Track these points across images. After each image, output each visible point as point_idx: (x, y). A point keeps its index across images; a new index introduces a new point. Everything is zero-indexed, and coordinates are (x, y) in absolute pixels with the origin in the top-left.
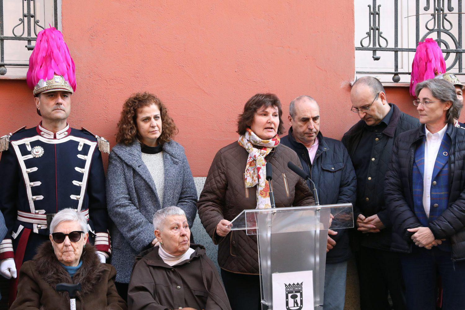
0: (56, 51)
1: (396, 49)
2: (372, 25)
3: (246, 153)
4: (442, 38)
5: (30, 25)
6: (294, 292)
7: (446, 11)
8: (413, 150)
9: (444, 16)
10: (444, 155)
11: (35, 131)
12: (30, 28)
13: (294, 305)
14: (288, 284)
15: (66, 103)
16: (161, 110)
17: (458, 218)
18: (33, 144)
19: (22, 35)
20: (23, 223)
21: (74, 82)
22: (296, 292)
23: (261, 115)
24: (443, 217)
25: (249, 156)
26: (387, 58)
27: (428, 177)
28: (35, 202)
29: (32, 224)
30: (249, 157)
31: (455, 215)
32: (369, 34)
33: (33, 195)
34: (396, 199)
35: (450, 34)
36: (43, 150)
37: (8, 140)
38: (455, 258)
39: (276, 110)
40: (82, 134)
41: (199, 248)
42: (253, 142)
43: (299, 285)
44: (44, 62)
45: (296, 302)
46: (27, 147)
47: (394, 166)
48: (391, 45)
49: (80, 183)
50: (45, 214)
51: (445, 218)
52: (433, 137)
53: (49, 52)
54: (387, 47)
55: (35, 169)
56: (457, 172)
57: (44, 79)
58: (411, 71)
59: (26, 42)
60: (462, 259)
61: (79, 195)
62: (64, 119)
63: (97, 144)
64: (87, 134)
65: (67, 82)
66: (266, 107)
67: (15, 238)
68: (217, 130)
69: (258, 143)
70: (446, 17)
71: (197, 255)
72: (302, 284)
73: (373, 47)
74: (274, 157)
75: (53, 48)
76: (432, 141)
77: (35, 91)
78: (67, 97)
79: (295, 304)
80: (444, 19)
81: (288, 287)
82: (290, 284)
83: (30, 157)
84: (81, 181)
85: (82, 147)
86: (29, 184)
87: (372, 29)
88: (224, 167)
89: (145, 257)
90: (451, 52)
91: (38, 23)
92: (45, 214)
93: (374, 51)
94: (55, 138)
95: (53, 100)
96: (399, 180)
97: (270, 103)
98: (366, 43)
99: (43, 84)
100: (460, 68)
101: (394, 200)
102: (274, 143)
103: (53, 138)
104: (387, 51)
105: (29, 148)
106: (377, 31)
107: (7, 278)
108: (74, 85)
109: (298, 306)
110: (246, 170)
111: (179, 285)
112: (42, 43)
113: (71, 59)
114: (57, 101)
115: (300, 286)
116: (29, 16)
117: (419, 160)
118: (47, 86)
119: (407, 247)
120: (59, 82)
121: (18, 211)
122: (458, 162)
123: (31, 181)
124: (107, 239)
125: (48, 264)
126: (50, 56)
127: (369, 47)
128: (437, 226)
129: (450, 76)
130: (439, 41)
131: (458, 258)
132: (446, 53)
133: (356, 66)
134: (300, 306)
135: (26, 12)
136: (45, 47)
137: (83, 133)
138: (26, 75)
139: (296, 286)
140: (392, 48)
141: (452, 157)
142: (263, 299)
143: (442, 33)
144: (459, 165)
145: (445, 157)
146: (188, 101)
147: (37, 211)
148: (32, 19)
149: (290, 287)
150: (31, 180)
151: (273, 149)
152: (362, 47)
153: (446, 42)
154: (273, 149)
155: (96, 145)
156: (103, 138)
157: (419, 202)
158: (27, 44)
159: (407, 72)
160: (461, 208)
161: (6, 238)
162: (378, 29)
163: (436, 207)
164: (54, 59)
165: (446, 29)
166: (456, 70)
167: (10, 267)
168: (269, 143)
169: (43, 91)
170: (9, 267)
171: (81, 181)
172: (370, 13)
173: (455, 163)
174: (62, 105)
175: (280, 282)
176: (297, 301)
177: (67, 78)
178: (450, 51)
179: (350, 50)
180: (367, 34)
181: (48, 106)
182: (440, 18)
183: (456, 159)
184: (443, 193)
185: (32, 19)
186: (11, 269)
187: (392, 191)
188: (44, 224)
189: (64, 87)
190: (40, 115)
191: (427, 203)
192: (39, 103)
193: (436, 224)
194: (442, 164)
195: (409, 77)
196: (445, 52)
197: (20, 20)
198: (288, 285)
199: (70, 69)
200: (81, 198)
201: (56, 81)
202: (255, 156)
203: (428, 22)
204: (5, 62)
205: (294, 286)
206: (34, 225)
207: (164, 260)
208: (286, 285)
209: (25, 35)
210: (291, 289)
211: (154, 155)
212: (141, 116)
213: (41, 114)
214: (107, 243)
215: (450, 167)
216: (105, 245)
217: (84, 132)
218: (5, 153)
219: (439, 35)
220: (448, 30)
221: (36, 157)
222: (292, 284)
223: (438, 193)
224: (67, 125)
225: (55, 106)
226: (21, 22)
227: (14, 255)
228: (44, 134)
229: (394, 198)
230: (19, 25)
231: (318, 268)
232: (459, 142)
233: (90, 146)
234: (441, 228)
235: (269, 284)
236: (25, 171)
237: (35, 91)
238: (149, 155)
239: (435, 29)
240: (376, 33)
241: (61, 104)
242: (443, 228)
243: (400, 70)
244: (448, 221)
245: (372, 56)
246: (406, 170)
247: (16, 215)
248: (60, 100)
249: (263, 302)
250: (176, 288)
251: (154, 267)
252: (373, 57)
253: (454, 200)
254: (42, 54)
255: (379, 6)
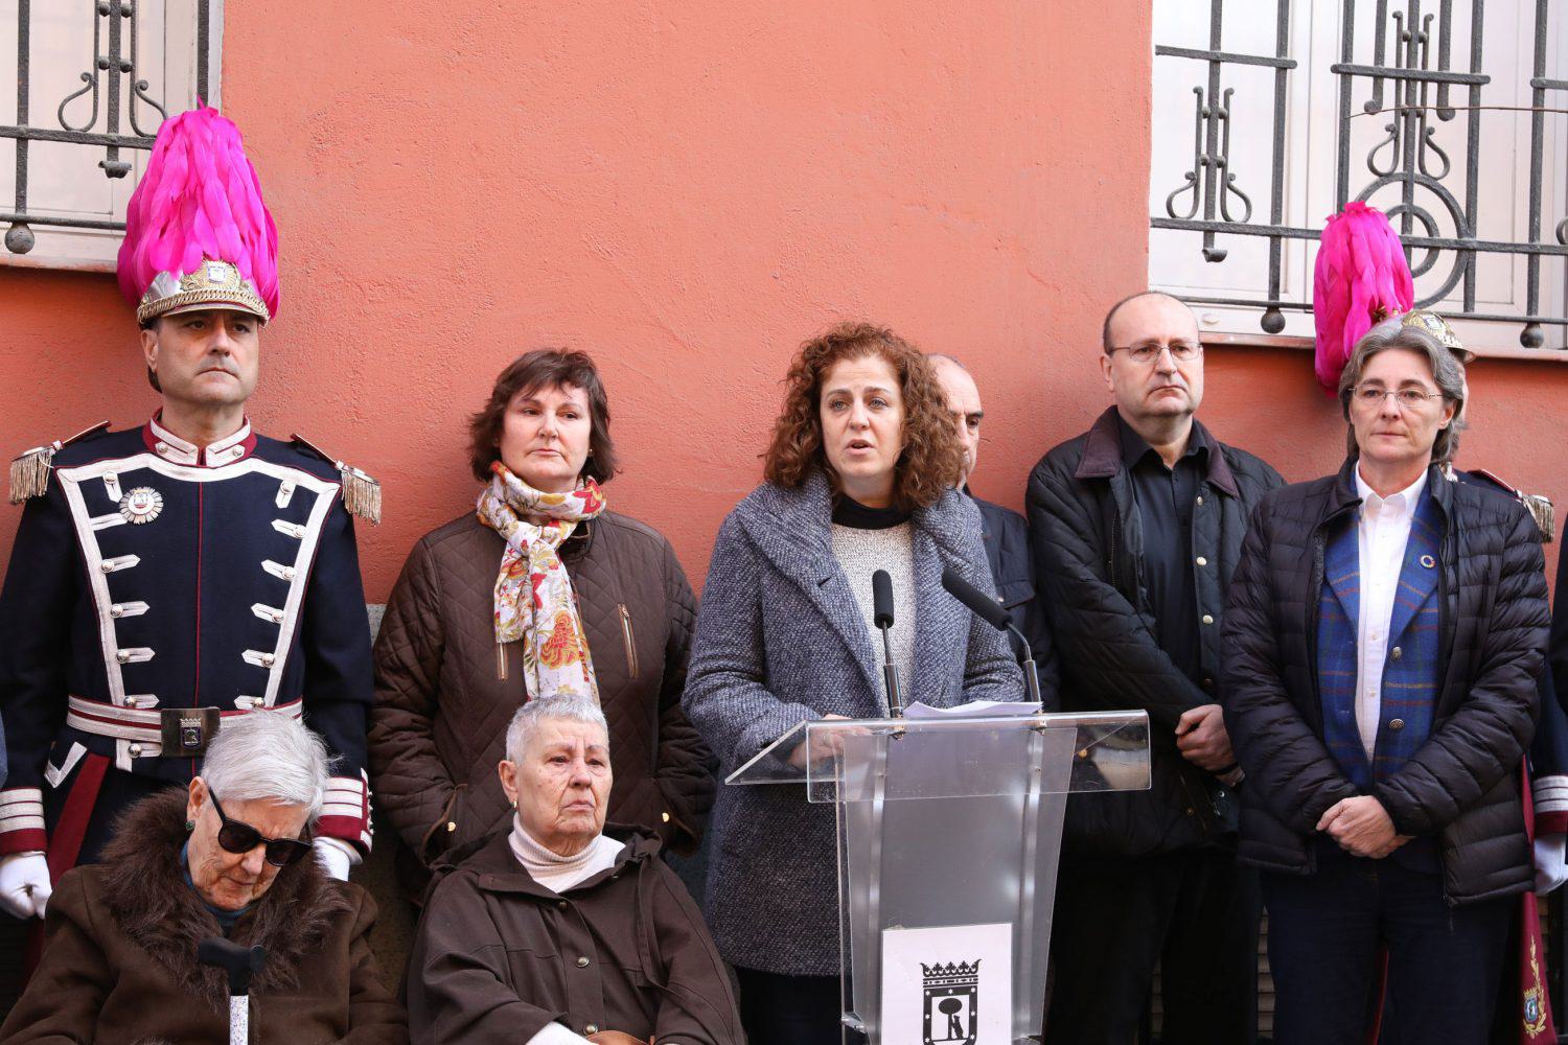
0: (213, 185)
1: (1277, 228)
2: (1204, 151)
3: (496, 540)
4: (1416, 203)
5: (118, 95)
6: (951, 991)
7: (1432, 118)
8: (1320, 547)
9: (1425, 133)
10: (1425, 565)
11: (138, 441)
12: (110, 110)
13: (950, 1033)
14: (931, 966)
15: (243, 352)
16: (903, 379)
17: (1468, 768)
18: (129, 481)
19: (89, 128)
20: (86, 738)
21: (274, 285)
22: (958, 991)
23: (523, 412)
24: (1421, 768)
25: (508, 548)
26: (1247, 257)
27: (1370, 633)
28: (128, 669)
29: (112, 741)
30: (506, 552)
31: (1458, 758)
32: (1193, 178)
33: (121, 646)
34: (1270, 699)
35: (1443, 192)
36: (160, 499)
37: (46, 464)
38: (1456, 894)
39: (578, 398)
40: (292, 454)
41: (638, 837)
42: (515, 505)
43: (940, 972)
44: (174, 216)
45: (955, 1025)
46: (108, 487)
47: (1255, 593)
48: (1262, 216)
49: (277, 613)
50: (156, 708)
51: (1429, 771)
52: (1385, 508)
53: (192, 184)
54: (1248, 223)
55: (131, 561)
56: (1465, 622)
57: (173, 270)
58: (1310, 301)
59: (101, 152)
60: (1476, 897)
61: (272, 650)
62: (235, 403)
63: (340, 490)
64: (309, 456)
65: (249, 283)
66: (537, 388)
67: (54, 786)
68: (709, 460)
69: (532, 507)
70: (1431, 137)
71: (636, 855)
72: (976, 965)
73: (1206, 218)
74: (588, 557)
75: (204, 176)
76: (1381, 519)
77: (143, 311)
78: (247, 330)
79: (953, 1030)
80: (1426, 145)
81: (931, 974)
82: (938, 965)
83: (116, 520)
84: (280, 605)
85: (289, 497)
86: (108, 610)
87: (1205, 163)
88: (433, 589)
89: (464, 865)
90: (1444, 248)
91: (143, 92)
92: (156, 708)
93: (1209, 232)
94: (202, 462)
95: (201, 341)
96: (1272, 639)
97: (550, 376)
98: (1183, 208)
99: (170, 288)
100: (1469, 300)
101: (1262, 701)
102: (583, 506)
103: (194, 462)
104: (1248, 234)
105: (114, 493)
106: (1219, 171)
107: (19, 916)
108: (273, 295)
109: (960, 1037)
110: (497, 587)
111: (582, 955)
112: (169, 154)
113: (266, 211)
114: (215, 342)
115: (970, 971)
116: (116, 66)
117: (1341, 579)
118: (182, 292)
119: (1301, 856)
120: (222, 282)
121: (71, 698)
122: (1469, 590)
123: (115, 600)
124: (359, 800)
125: (149, 881)
126: (193, 198)
127: (1193, 219)
128: (1405, 792)
129: (1425, 321)
130: (1408, 212)
131: (1467, 895)
132: (1427, 250)
133: (1150, 282)
134: (968, 1039)
135: (104, 53)
136: (181, 168)
137: (298, 453)
138: (116, 259)
139: (957, 972)
140: (1264, 227)
141: (1451, 573)
142: (849, 1009)
143: (1416, 185)
144: (1470, 598)
145: (1426, 571)
146: (622, 364)
147: (131, 699)
148: (125, 78)
149: (938, 974)
150: (116, 598)
151: (582, 526)
152: (1559, 244)
153: (1428, 215)
154: (582, 526)
155: (334, 493)
156: (358, 472)
157: (1343, 712)
158: (104, 158)
159: (1302, 302)
160: (1477, 737)
161: (13, 783)
162: (1222, 165)
163: (1397, 730)
164: (204, 206)
165: (1428, 175)
166: (1454, 303)
167: (32, 883)
168: (566, 502)
169: (168, 311)
170: (28, 879)
171: (280, 605)
172: (1198, 113)
173: (1458, 593)
174: (231, 357)
175: (906, 957)
176: (961, 1020)
177: (248, 271)
178: (1441, 245)
179: (1130, 225)
180: (1187, 177)
181: (183, 356)
182: (1414, 138)
183: (1461, 583)
184: (1420, 686)
185: (125, 78)
186: (35, 890)
187: (1253, 673)
188: (151, 740)
189: (238, 299)
190: (158, 389)
191: (1368, 714)
192: (156, 348)
193: (1400, 786)
194: (1419, 592)
195: (1311, 318)
196: (1425, 247)
197: (85, 77)
198: (931, 967)
199: (259, 243)
200: (276, 661)
201: (212, 277)
202: (525, 541)
203: (1377, 148)
204: (30, 213)
205: (951, 973)
206: (118, 742)
207: (532, 874)
208: (925, 969)
209: (101, 128)
210: (941, 982)
211: (877, 532)
212: (831, 388)
213: (162, 385)
214: (358, 813)
215: (1445, 603)
216: (349, 820)
217: (299, 449)
218: (35, 505)
219: (1407, 193)
220: (1436, 179)
221: (137, 521)
222: (957, 965)
223: (1405, 685)
224: (244, 423)
225: (206, 358)
226: (86, 84)
227: (45, 841)
228: (165, 451)
229: (1263, 694)
230: (81, 93)
231: (1028, 915)
232: (1469, 528)
233: (316, 495)
234: (1418, 799)
235: (870, 963)
236: (98, 566)
237: (143, 311)
238: (859, 531)
239: (1396, 172)
240: (1215, 177)
241: (227, 354)
242: (1424, 801)
243: (1283, 298)
244: (1437, 778)
245: (1202, 248)
246: (1297, 609)
247: (65, 709)
248: (224, 340)
249: (847, 1020)
250: (577, 964)
251: (501, 896)
252: (1205, 251)
253: (1452, 711)
254: (168, 191)
255: (1229, 93)
